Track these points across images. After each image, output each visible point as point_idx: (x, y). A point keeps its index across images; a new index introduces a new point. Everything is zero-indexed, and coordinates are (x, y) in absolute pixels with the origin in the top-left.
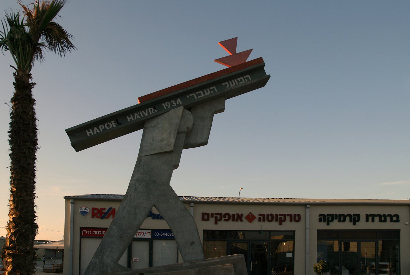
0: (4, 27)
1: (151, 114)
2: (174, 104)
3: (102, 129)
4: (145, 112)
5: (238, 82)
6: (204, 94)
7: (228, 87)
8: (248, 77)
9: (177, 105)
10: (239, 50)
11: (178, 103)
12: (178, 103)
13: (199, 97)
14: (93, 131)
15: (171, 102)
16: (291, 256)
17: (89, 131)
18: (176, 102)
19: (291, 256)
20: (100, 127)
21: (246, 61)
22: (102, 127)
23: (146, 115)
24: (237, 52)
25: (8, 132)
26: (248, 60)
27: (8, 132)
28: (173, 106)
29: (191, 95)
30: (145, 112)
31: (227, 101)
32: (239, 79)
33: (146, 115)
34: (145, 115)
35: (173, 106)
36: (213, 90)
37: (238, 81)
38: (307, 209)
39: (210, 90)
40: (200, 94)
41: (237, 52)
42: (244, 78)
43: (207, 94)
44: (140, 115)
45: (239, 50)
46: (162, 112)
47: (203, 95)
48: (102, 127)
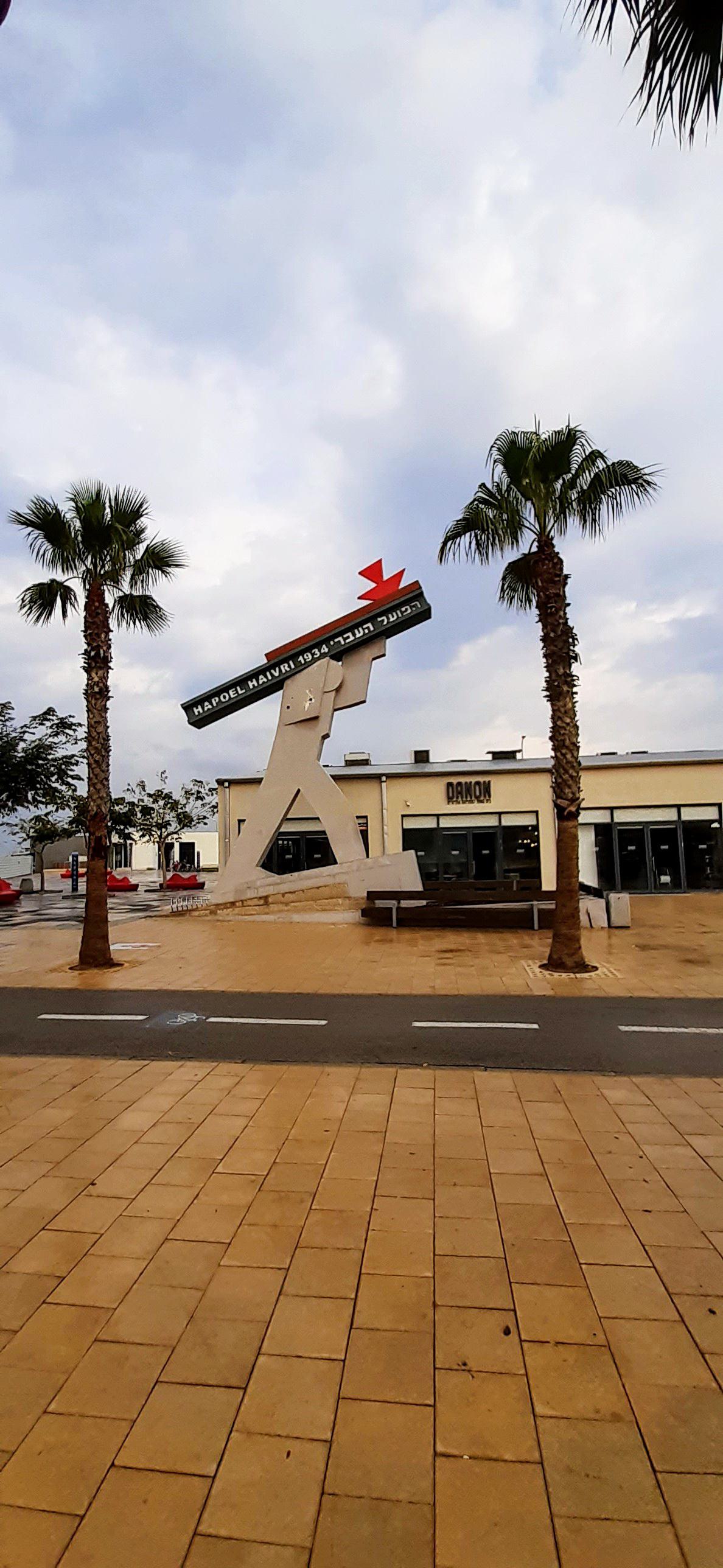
0: (602, 22)
1: (284, 671)
2: (317, 654)
3: (217, 703)
4: (275, 671)
5: (402, 613)
6: (354, 635)
7: (385, 623)
8: (416, 604)
9: (321, 654)
10: (386, 576)
11: (322, 651)
12: (322, 651)
13: (347, 641)
14: (203, 708)
15: (313, 651)
16: (545, 888)
17: (197, 708)
18: (320, 651)
19: (545, 888)
20: (213, 700)
21: (399, 585)
22: (215, 700)
23: (277, 674)
24: (386, 577)
25: (569, 605)
26: (402, 586)
27: (569, 605)
28: (315, 656)
29: (336, 640)
30: (275, 671)
31: (388, 641)
32: (403, 609)
33: (277, 674)
34: (274, 676)
35: (315, 656)
36: (368, 628)
37: (401, 611)
38: (384, 784)
39: (363, 629)
40: (348, 637)
41: (386, 577)
42: (343, 638)
43: (358, 635)
44: (266, 677)
45: (386, 576)
46: (300, 668)
47: (352, 638)
48: (215, 700)
